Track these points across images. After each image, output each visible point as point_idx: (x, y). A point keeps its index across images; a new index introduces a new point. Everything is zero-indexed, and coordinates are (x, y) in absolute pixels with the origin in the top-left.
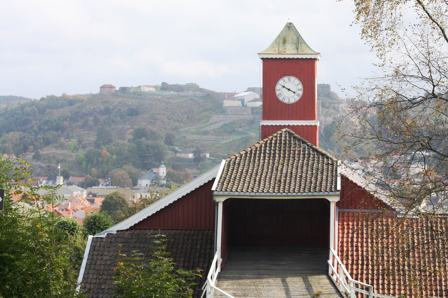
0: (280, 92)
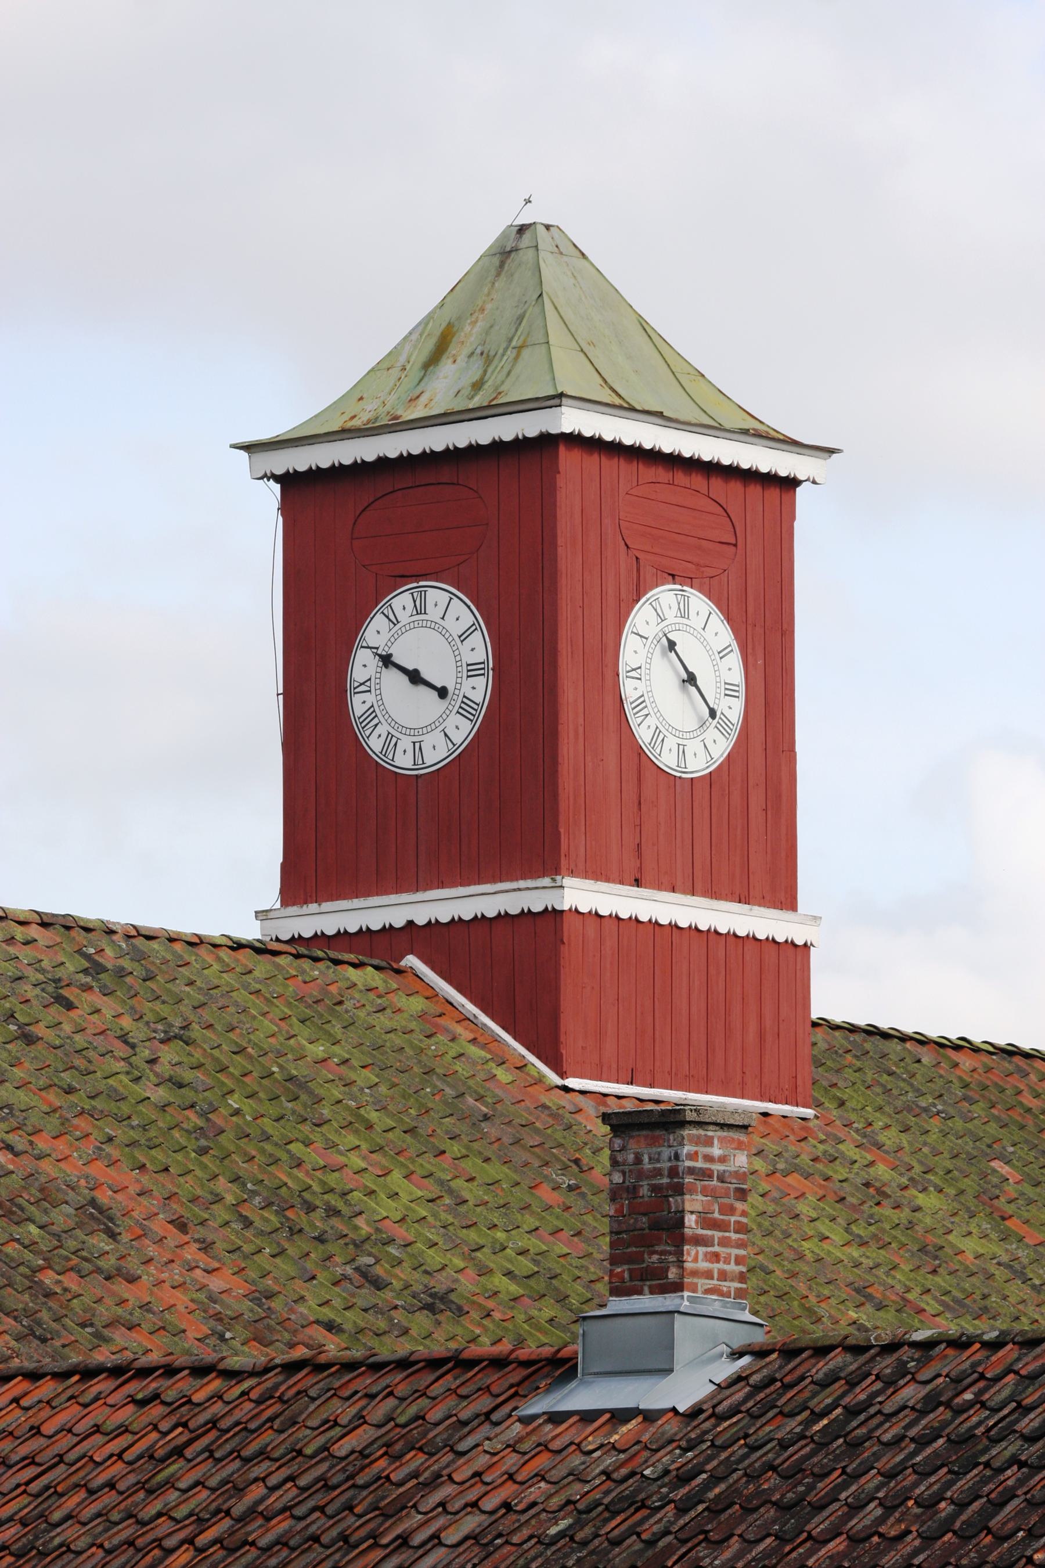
0: (370, 698)
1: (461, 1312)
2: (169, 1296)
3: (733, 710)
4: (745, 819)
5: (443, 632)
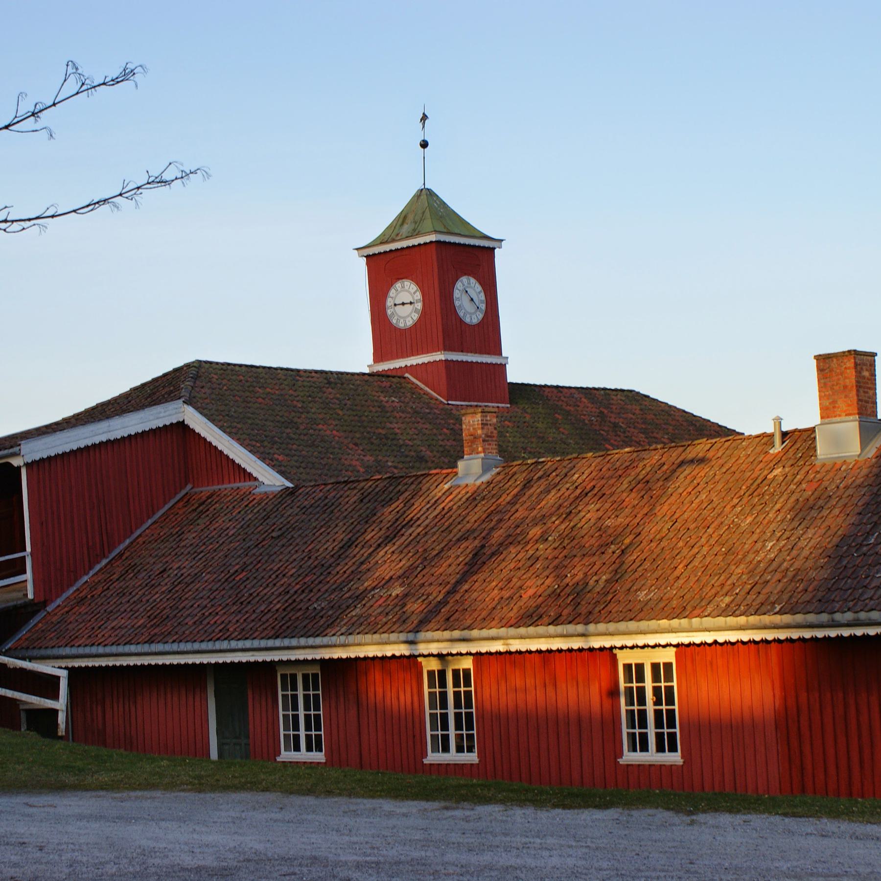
1: (427, 462)
2: (354, 463)
3: (483, 307)
4: (488, 334)
5: (409, 292)
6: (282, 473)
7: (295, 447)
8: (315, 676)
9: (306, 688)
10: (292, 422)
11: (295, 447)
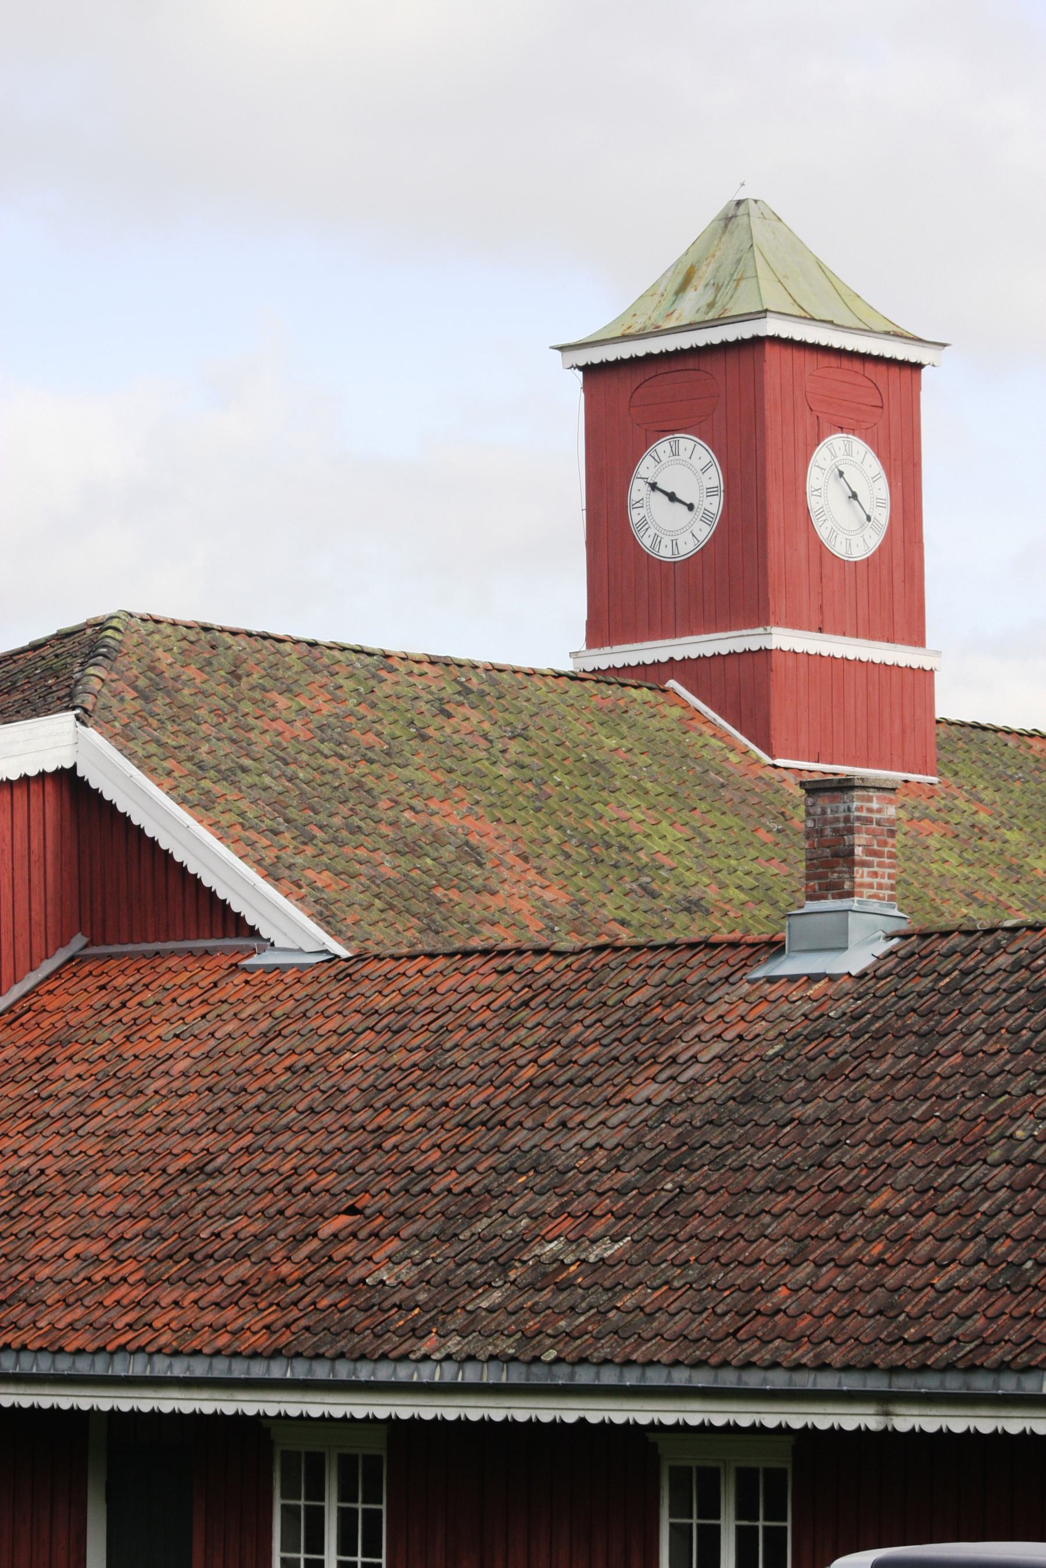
0: (643, 512)
1: (708, 912)
2: (517, 903)
3: (882, 516)
4: (891, 589)
6: (325, 919)
7: (362, 853)
8: (775, 1477)
9: (746, 1510)
10: (360, 785)
11: (362, 853)
